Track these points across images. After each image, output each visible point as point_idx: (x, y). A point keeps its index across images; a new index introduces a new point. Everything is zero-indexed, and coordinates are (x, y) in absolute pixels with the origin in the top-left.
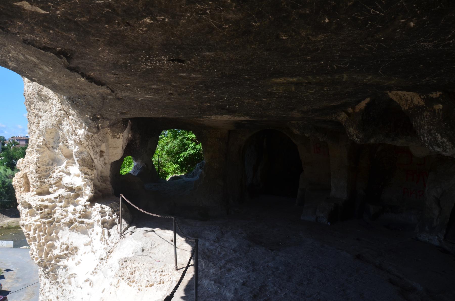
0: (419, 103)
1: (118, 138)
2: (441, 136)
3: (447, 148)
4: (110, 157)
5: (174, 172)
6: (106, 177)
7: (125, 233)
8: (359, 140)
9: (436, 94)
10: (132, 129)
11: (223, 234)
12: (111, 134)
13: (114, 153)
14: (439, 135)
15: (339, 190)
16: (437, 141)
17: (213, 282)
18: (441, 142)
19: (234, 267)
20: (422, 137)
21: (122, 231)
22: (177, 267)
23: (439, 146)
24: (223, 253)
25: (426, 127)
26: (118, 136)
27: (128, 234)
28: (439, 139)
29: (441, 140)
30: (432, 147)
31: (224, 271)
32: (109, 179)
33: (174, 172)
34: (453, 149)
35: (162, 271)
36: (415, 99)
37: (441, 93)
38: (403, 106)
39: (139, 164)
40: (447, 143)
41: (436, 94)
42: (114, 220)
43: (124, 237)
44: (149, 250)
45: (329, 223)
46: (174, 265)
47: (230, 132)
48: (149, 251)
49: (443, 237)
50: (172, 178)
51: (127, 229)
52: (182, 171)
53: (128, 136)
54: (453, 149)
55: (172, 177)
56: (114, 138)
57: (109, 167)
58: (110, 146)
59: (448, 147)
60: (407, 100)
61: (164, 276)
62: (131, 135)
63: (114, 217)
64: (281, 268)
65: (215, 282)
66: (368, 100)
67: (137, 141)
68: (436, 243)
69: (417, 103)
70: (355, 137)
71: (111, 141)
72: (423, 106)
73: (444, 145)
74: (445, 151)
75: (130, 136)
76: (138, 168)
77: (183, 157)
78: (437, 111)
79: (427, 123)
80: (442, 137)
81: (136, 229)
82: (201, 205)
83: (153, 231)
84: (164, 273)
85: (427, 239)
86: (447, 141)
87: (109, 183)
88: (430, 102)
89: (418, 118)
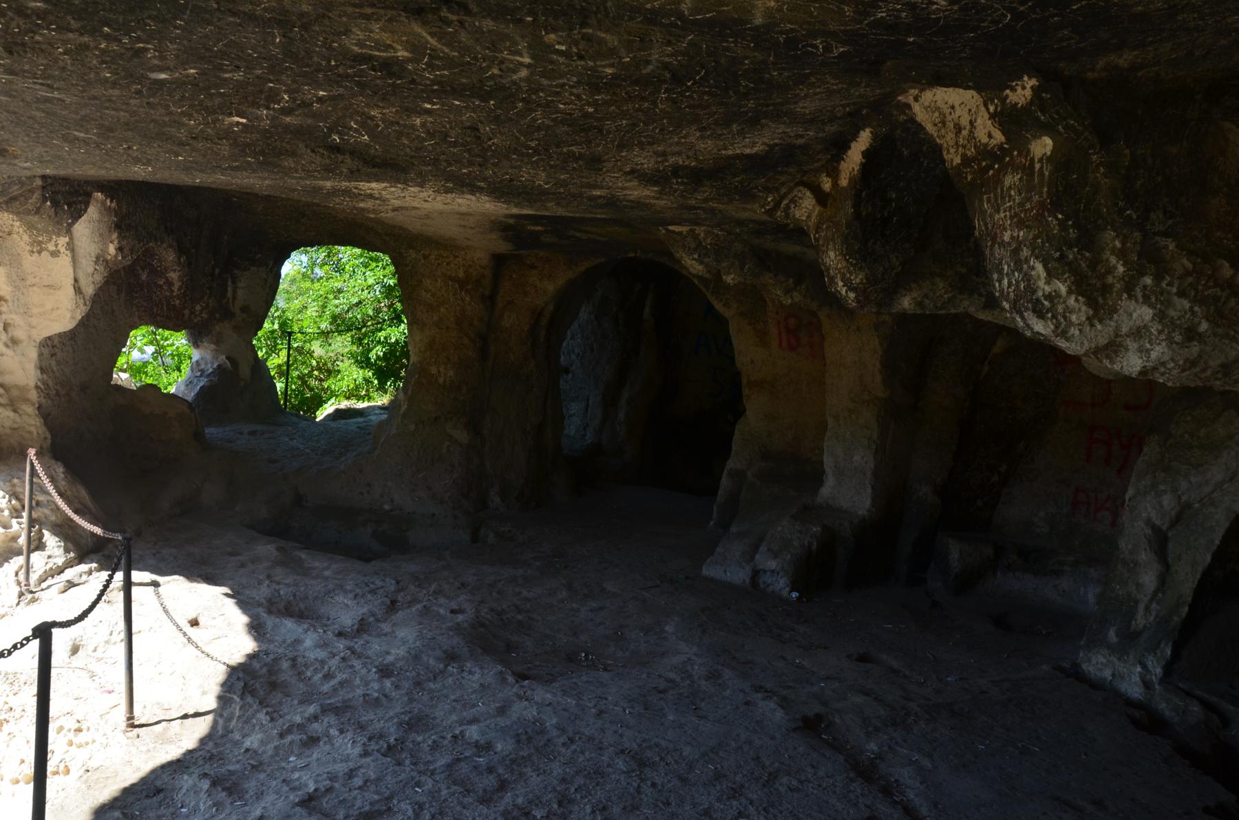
0: (990, 136)
1: (55, 254)
2: (1045, 266)
3: (1070, 324)
4: (34, 321)
5: (352, 394)
6: (22, 389)
7: (44, 585)
8: (852, 295)
9: (1024, 88)
10: (122, 225)
11: (393, 606)
12: (26, 237)
13: (49, 306)
14: (1039, 267)
15: (848, 485)
16: (1034, 292)
17: (205, 785)
18: (1048, 297)
19: (334, 732)
20: (995, 276)
21: (34, 577)
22: (131, 717)
23: (1041, 315)
24: (340, 677)
25: (1007, 237)
26: (51, 247)
27: (55, 589)
28: (1041, 283)
29: (1047, 289)
30: (1023, 318)
31: (291, 743)
32: (33, 395)
33: (352, 394)
34: (1092, 325)
35: (79, 730)
36: (979, 121)
37: (1034, 82)
38: (948, 152)
39: (209, 357)
40: (1071, 301)
41: (1024, 88)
42: (15, 538)
43: (34, 600)
44: (100, 650)
45: (795, 595)
46: (121, 714)
47: (499, 260)
48: (99, 654)
49: (1159, 671)
50: (339, 414)
51: (62, 572)
52: (382, 388)
53: (105, 250)
54: (1092, 325)
55: (337, 411)
56: (39, 252)
57: (33, 354)
58: (30, 280)
59: (1074, 318)
60: (958, 129)
61: (80, 746)
62: (120, 249)
63: (15, 527)
64: (499, 747)
65: (214, 784)
66: (864, 139)
67: (173, 276)
68: (1134, 690)
69: (985, 140)
70: (841, 284)
71: (30, 261)
72: (1001, 147)
73: (1060, 308)
74: (1064, 334)
75: (112, 249)
76: (202, 371)
77: (385, 343)
78: (1037, 166)
79: (1011, 218)
80: (1051, 275)
81: (95, 574)
82: (387, 507)
83: (155, 584)
84: (81, 738)
85: (1107, 674)
86: (1070, 292)
87: (30, 410)
88: (1014, 122)
89: (989, 201)
